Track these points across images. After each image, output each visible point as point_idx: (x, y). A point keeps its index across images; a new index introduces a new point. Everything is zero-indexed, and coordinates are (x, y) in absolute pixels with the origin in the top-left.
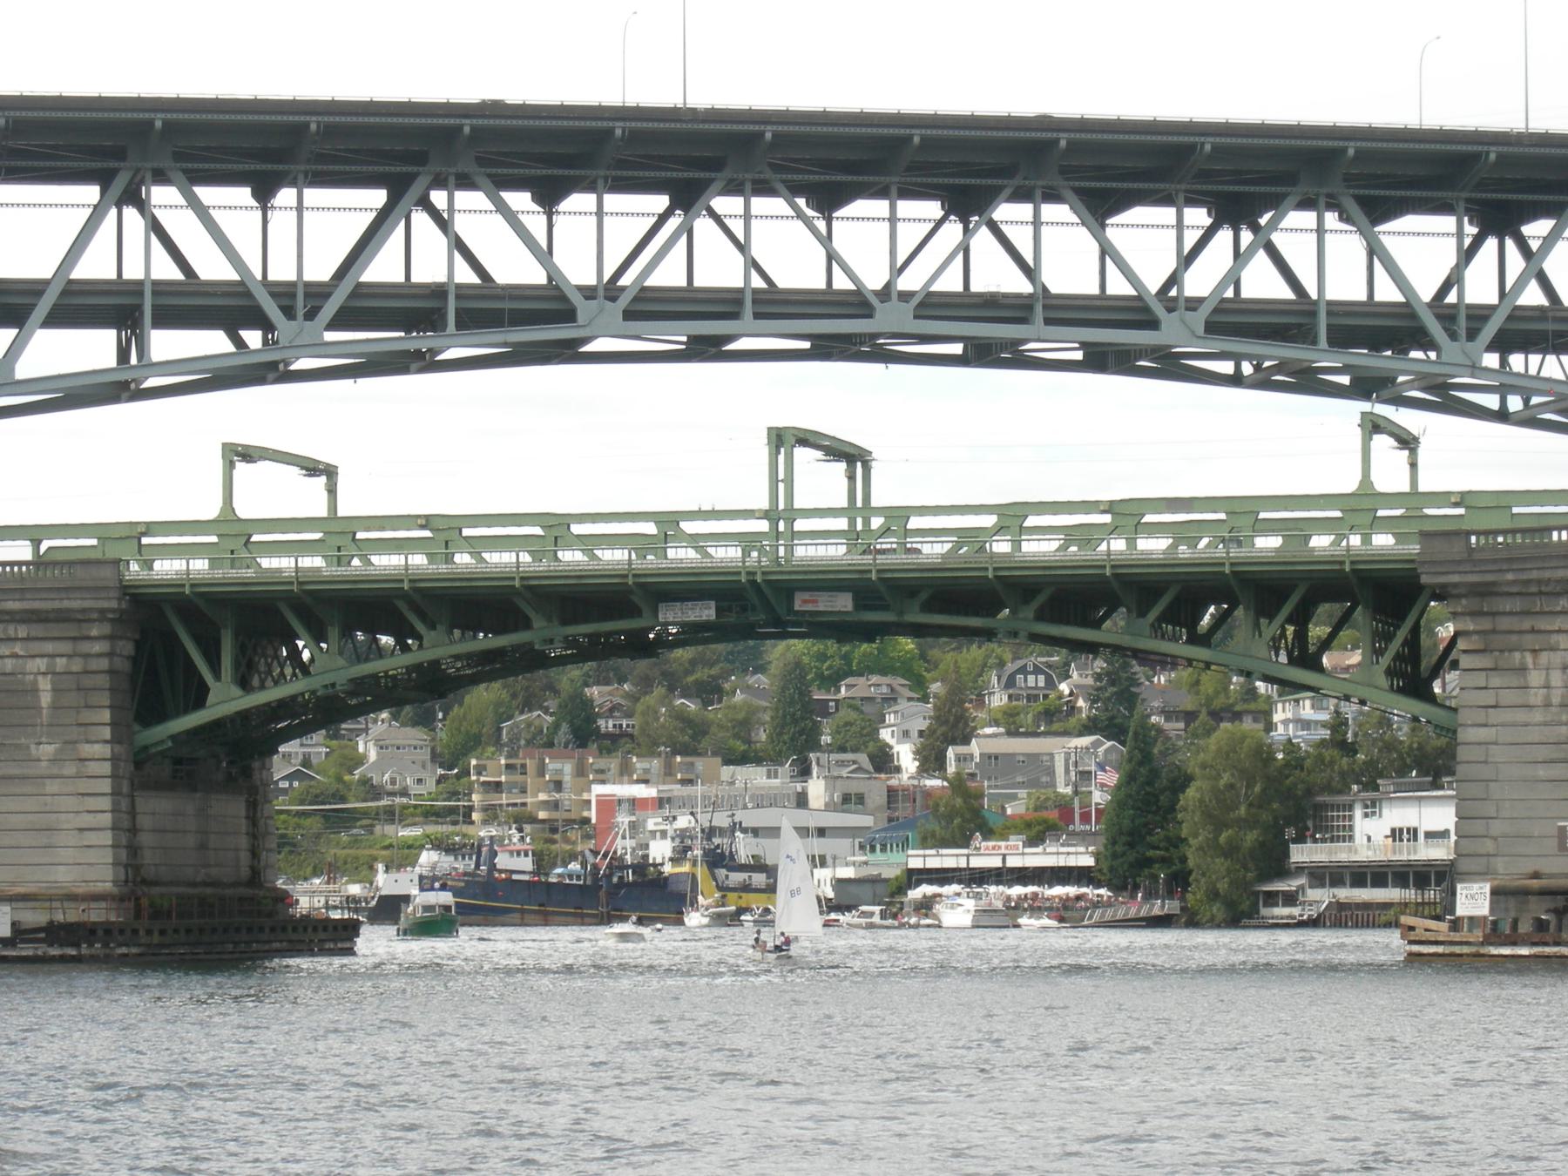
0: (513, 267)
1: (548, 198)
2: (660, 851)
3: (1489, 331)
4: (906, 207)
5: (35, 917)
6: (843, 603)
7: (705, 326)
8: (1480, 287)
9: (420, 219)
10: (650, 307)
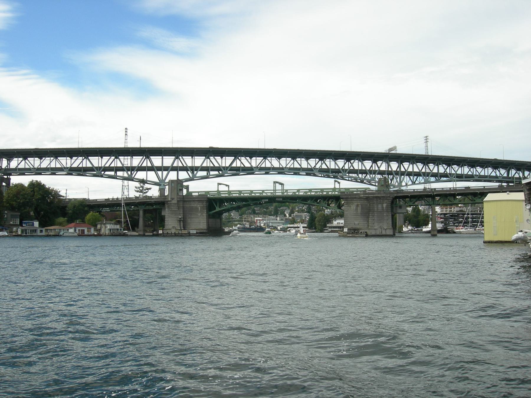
0: (247, 165)
1: (251, 158)
2: (262, 225)
3: (347, 171)
4: (287, 159)
5: (198, 231)
6: (281, 199)
7: (267, 171)
8: (346, 167)
9: (238, 160)
10: (261, 169)
